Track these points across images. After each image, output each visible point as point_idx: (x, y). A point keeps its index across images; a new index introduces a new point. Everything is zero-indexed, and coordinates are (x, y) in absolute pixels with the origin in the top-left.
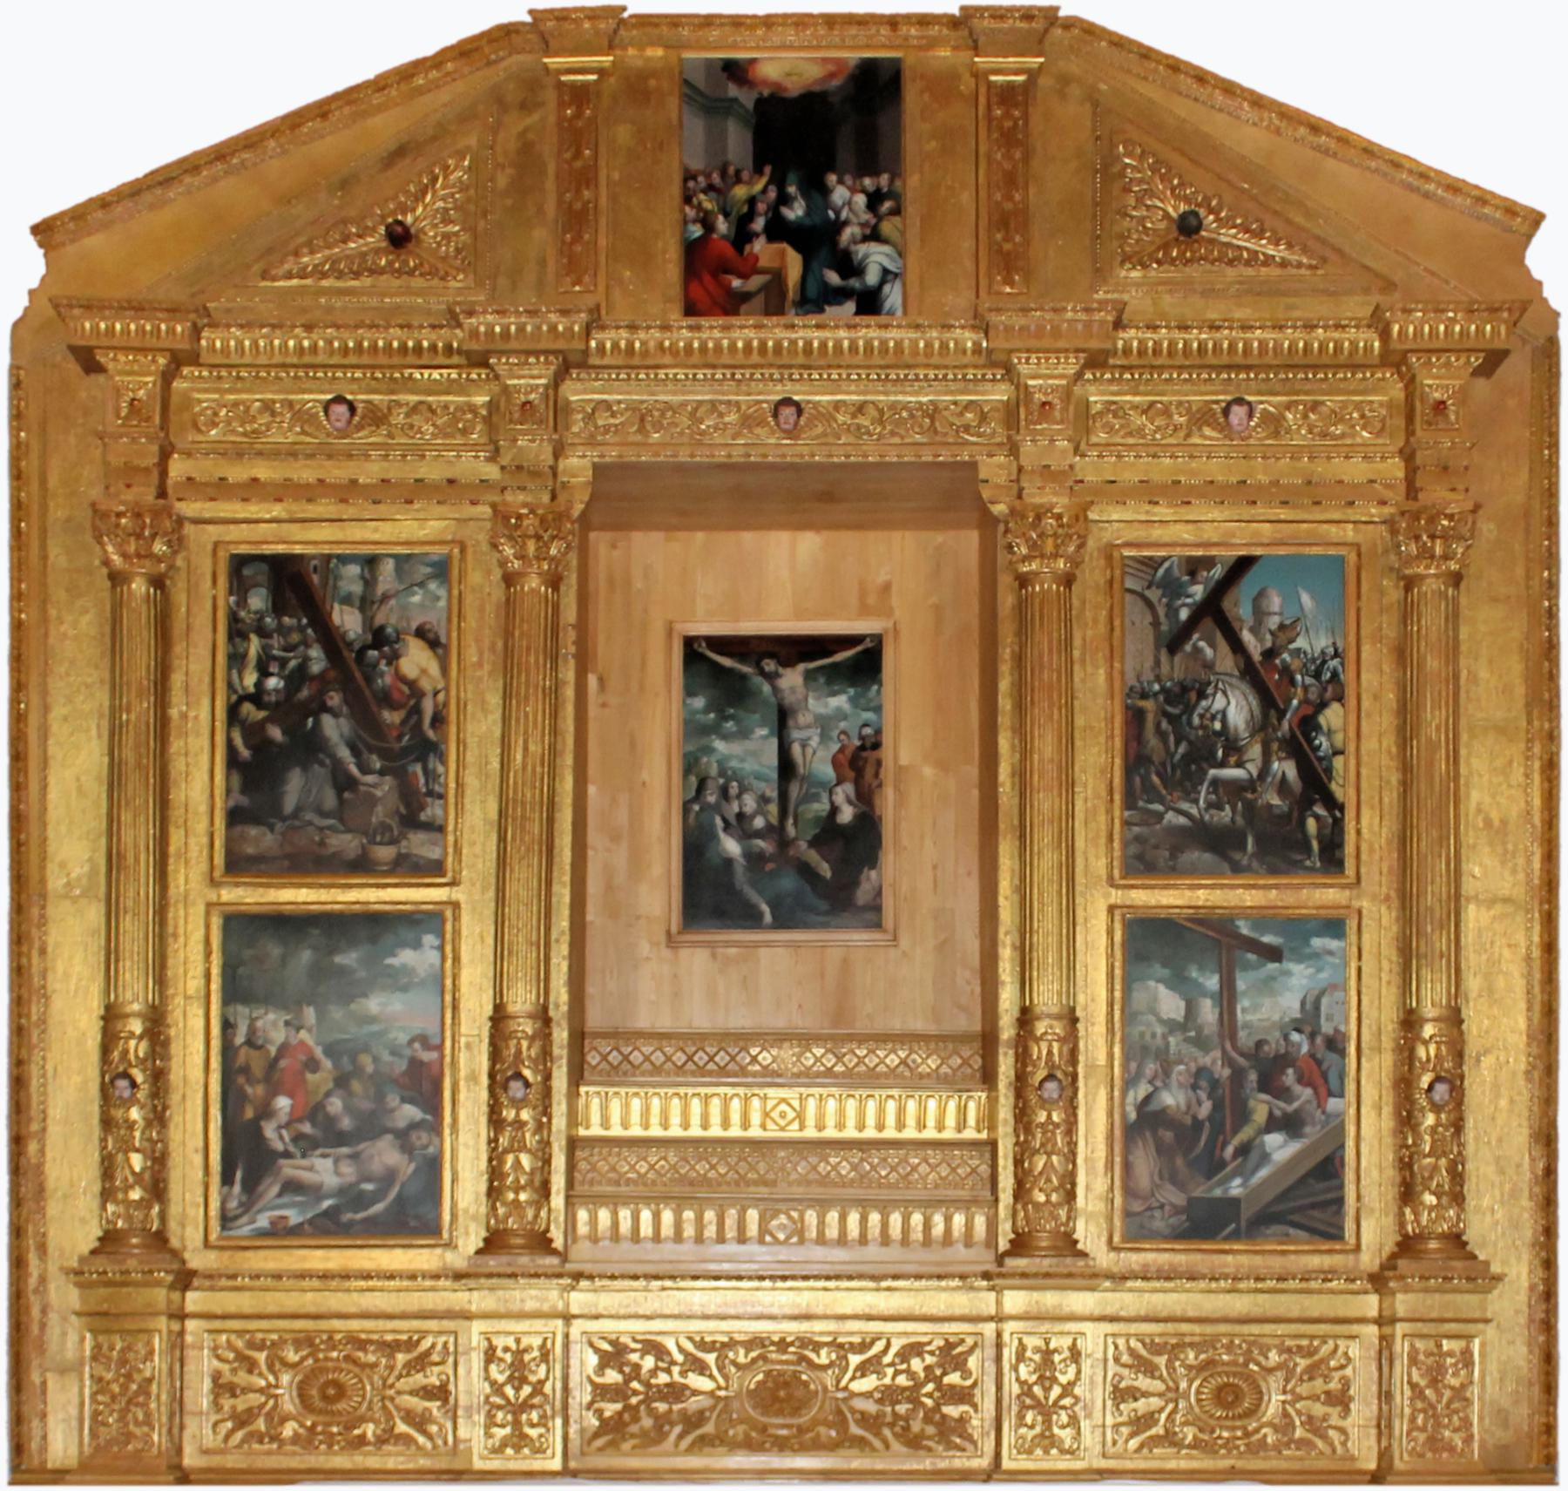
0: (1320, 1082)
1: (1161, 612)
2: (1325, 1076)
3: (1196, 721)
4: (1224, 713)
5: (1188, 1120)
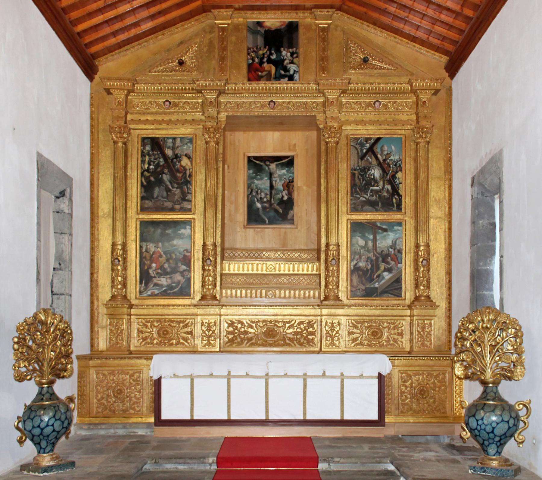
0: (396, 260)
1: (359, 150)
2: (397, 259)
3: (367, 176)
4: (374, 174)
5: (365, 269)
